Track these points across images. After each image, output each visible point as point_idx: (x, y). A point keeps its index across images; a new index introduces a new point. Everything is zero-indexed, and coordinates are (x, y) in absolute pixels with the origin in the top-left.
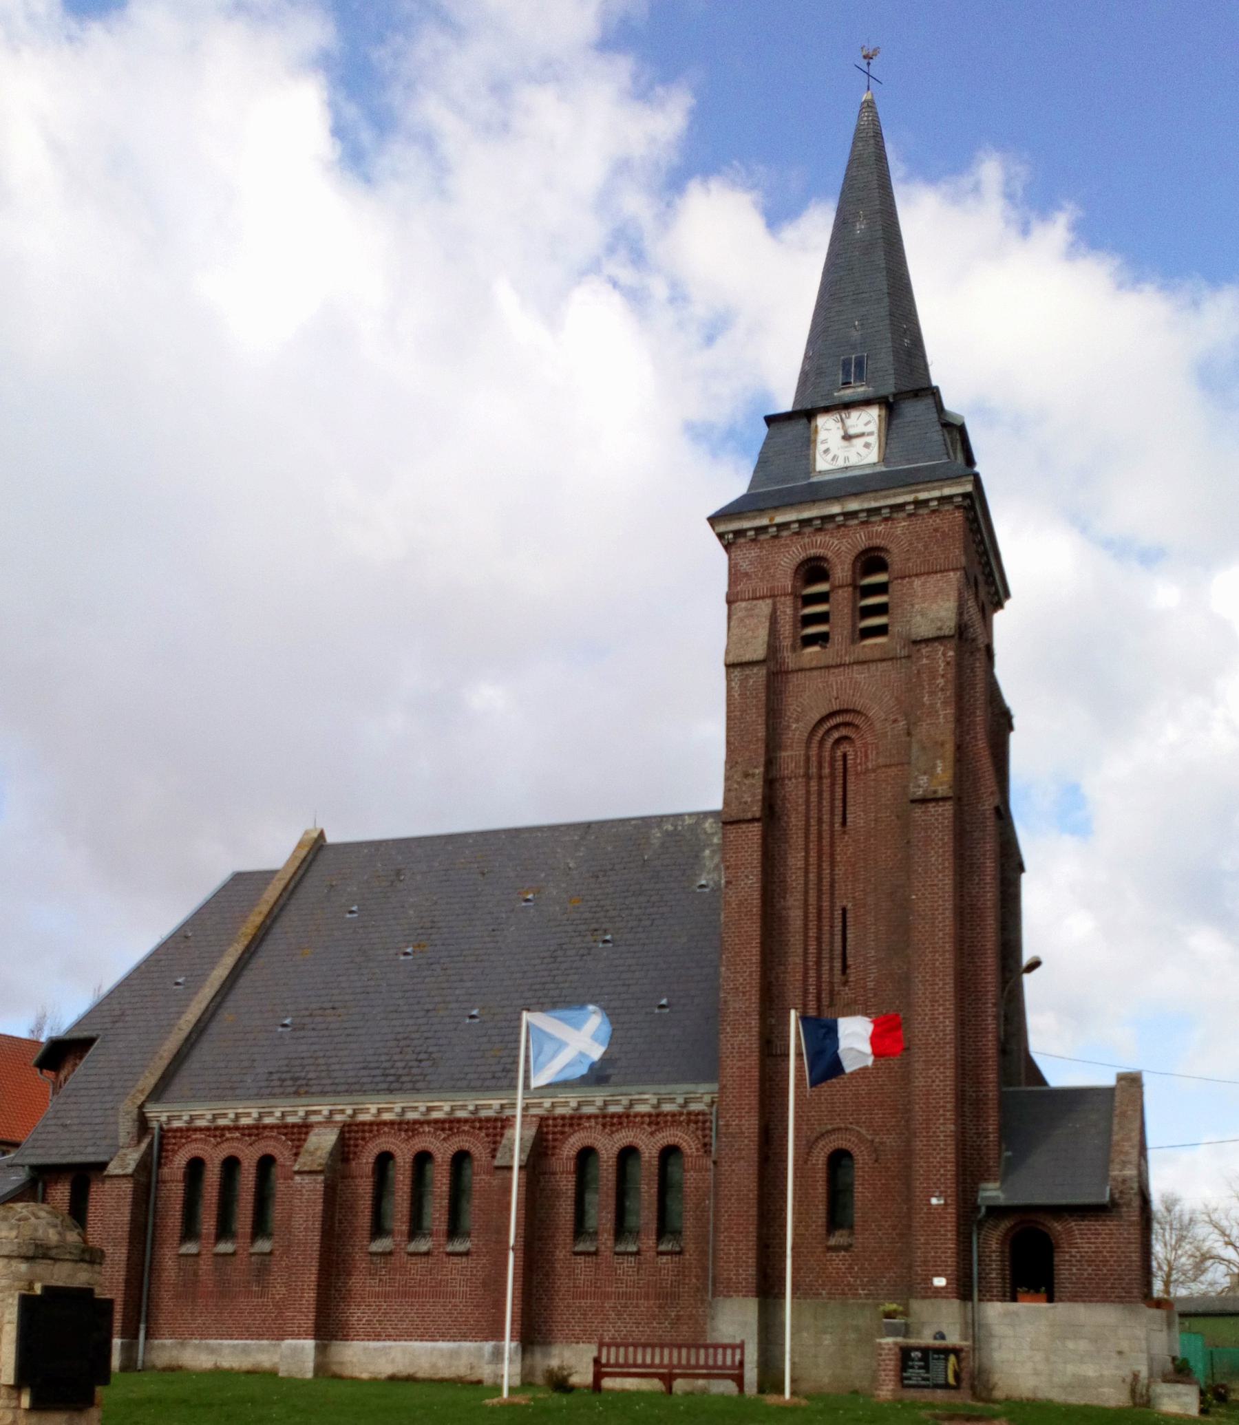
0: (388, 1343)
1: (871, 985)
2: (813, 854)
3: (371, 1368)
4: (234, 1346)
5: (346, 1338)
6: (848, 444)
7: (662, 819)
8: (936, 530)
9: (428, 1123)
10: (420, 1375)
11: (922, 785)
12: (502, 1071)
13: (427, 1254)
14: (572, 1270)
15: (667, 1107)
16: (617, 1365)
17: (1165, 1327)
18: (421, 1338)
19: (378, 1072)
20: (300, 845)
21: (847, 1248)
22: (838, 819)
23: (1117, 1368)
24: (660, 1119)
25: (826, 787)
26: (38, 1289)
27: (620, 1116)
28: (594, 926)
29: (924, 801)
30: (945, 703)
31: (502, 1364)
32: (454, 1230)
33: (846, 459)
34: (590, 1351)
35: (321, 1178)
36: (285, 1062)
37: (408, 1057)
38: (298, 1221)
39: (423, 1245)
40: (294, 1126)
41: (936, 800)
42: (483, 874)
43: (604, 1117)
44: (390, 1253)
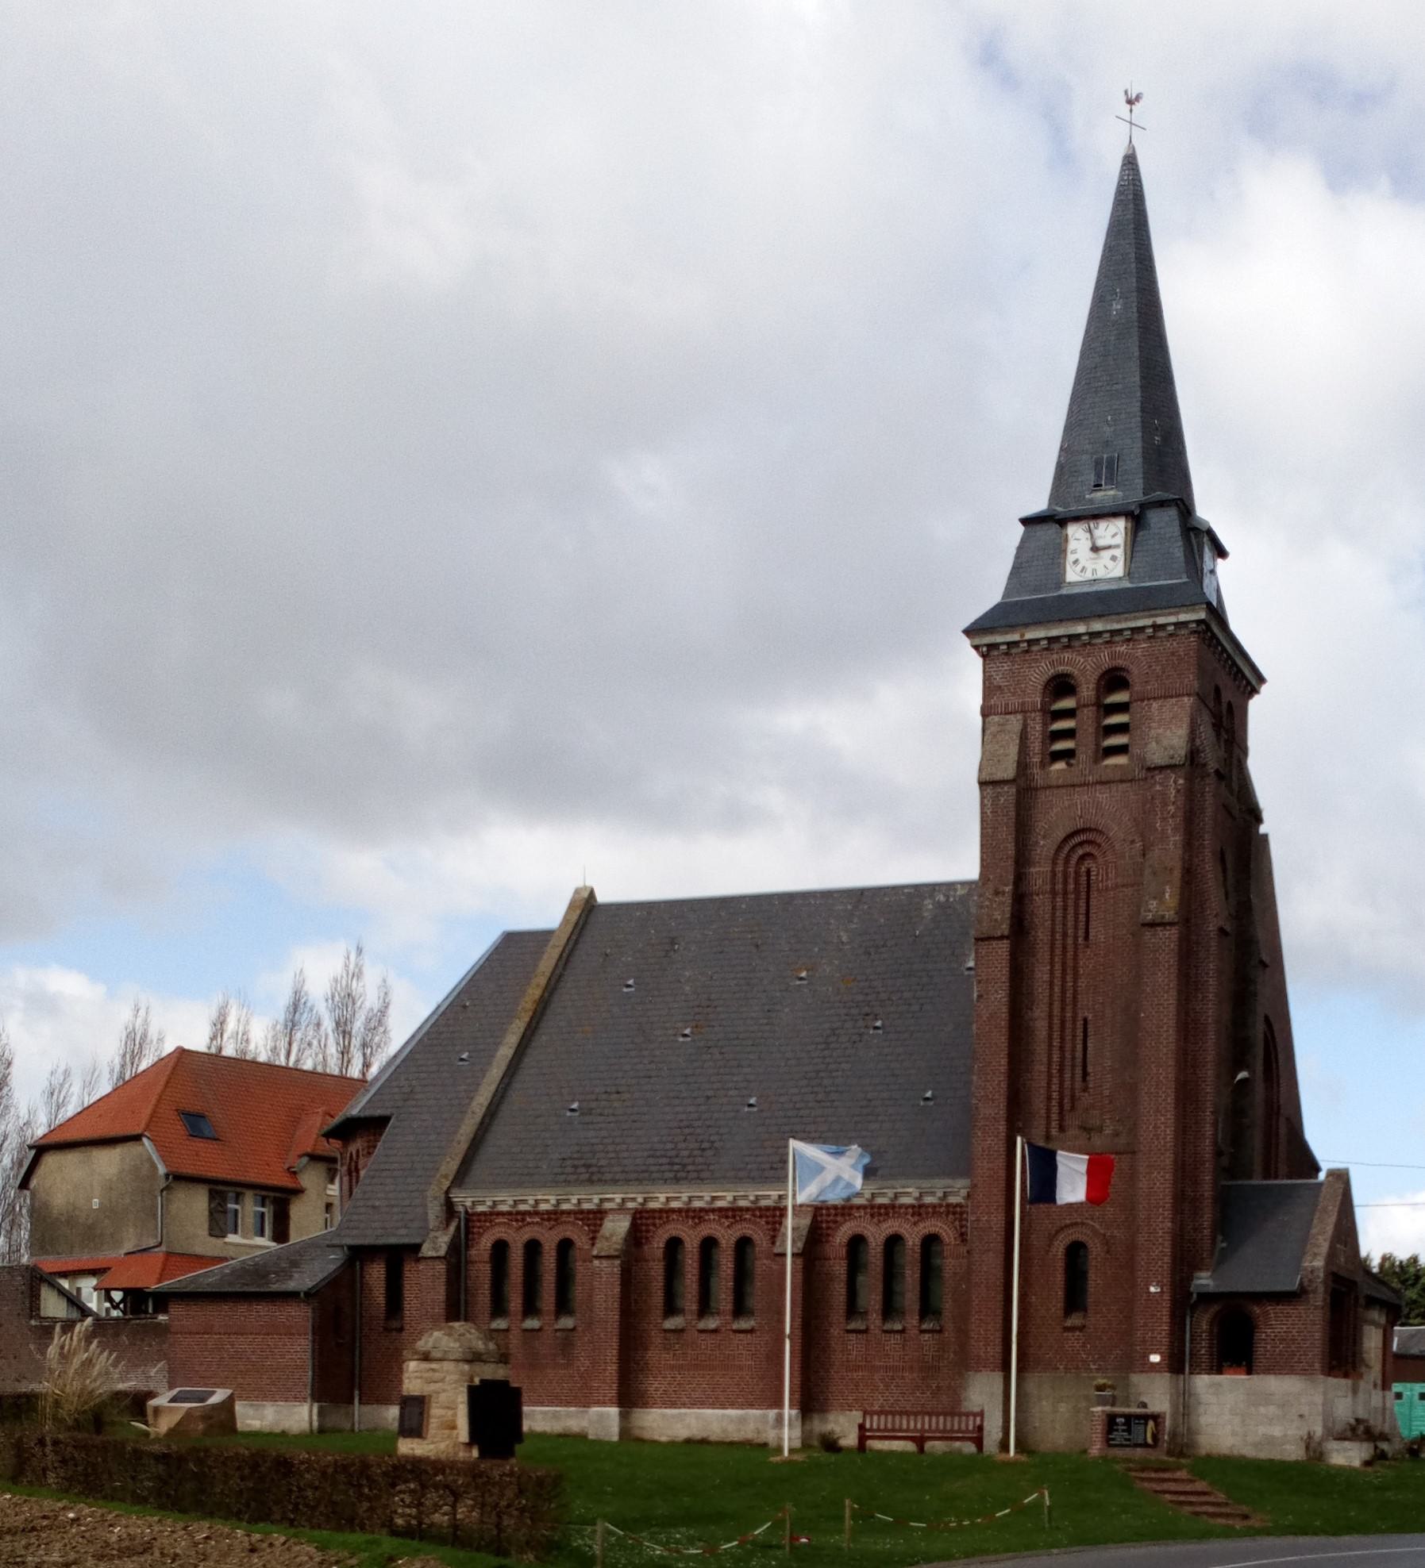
0: (683, 1411)
1: (1107, 1093)
2: (1058, 967)
3: (670, 1433)
4: (545, 1413)
5: (645, 1405)
6: (1096, 556)
7: (934, 888)
8: (1173, 654)
9: (713, 1210)
10: (713, 1438)
11: (1153, 909)
12: (775, 1169)
13: (715, 1331)
14: (845, 1346)
15: (928, 1200)
16: (879, 1430)
17: (1350, 1394)
18: (713, 1406)
19: (664, 1160)
20: (572, 906)
21: (1082, 1328)
22: (1081, 933)
23: (1298, 1428)
24: (923, 1210)
25: (1071, 903)
26: (477, 1381)
27: (885, 1206)
28: (867, 1010)
29: (1152, 925)
30: (1175, 830)
31: (782, 1429)
32: (740, 1309)
33: (1094, 571)
34: (857, 1416)
35: (617, 1262)
36: (577, 1148)
37: (692, 1146)
38: (599, 1298)
39: (712, 1323)
40: (589, 1212)
41: (1163, 925)
42: (757, 946)
43: (872, 1207)
44: (682, 1330)
